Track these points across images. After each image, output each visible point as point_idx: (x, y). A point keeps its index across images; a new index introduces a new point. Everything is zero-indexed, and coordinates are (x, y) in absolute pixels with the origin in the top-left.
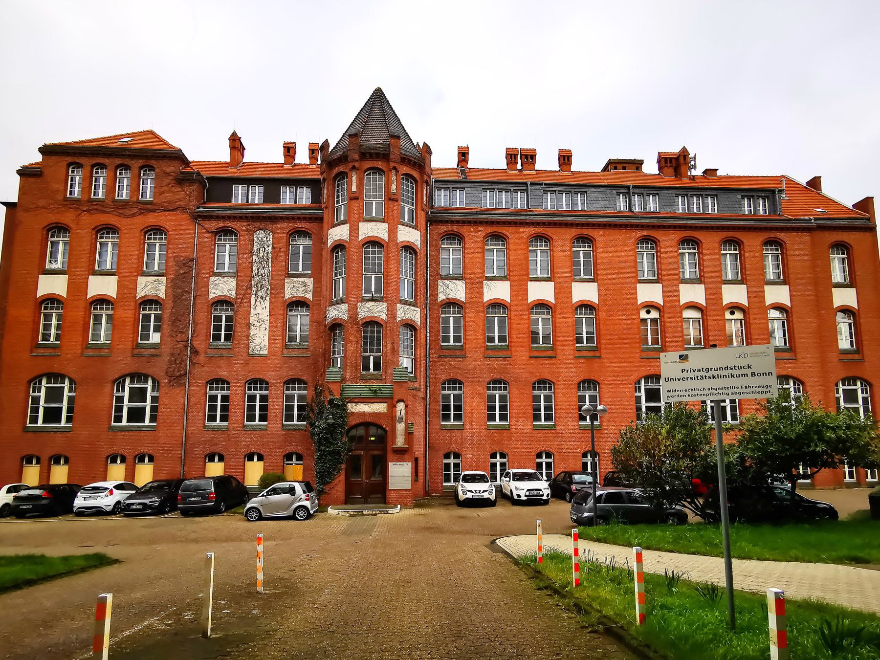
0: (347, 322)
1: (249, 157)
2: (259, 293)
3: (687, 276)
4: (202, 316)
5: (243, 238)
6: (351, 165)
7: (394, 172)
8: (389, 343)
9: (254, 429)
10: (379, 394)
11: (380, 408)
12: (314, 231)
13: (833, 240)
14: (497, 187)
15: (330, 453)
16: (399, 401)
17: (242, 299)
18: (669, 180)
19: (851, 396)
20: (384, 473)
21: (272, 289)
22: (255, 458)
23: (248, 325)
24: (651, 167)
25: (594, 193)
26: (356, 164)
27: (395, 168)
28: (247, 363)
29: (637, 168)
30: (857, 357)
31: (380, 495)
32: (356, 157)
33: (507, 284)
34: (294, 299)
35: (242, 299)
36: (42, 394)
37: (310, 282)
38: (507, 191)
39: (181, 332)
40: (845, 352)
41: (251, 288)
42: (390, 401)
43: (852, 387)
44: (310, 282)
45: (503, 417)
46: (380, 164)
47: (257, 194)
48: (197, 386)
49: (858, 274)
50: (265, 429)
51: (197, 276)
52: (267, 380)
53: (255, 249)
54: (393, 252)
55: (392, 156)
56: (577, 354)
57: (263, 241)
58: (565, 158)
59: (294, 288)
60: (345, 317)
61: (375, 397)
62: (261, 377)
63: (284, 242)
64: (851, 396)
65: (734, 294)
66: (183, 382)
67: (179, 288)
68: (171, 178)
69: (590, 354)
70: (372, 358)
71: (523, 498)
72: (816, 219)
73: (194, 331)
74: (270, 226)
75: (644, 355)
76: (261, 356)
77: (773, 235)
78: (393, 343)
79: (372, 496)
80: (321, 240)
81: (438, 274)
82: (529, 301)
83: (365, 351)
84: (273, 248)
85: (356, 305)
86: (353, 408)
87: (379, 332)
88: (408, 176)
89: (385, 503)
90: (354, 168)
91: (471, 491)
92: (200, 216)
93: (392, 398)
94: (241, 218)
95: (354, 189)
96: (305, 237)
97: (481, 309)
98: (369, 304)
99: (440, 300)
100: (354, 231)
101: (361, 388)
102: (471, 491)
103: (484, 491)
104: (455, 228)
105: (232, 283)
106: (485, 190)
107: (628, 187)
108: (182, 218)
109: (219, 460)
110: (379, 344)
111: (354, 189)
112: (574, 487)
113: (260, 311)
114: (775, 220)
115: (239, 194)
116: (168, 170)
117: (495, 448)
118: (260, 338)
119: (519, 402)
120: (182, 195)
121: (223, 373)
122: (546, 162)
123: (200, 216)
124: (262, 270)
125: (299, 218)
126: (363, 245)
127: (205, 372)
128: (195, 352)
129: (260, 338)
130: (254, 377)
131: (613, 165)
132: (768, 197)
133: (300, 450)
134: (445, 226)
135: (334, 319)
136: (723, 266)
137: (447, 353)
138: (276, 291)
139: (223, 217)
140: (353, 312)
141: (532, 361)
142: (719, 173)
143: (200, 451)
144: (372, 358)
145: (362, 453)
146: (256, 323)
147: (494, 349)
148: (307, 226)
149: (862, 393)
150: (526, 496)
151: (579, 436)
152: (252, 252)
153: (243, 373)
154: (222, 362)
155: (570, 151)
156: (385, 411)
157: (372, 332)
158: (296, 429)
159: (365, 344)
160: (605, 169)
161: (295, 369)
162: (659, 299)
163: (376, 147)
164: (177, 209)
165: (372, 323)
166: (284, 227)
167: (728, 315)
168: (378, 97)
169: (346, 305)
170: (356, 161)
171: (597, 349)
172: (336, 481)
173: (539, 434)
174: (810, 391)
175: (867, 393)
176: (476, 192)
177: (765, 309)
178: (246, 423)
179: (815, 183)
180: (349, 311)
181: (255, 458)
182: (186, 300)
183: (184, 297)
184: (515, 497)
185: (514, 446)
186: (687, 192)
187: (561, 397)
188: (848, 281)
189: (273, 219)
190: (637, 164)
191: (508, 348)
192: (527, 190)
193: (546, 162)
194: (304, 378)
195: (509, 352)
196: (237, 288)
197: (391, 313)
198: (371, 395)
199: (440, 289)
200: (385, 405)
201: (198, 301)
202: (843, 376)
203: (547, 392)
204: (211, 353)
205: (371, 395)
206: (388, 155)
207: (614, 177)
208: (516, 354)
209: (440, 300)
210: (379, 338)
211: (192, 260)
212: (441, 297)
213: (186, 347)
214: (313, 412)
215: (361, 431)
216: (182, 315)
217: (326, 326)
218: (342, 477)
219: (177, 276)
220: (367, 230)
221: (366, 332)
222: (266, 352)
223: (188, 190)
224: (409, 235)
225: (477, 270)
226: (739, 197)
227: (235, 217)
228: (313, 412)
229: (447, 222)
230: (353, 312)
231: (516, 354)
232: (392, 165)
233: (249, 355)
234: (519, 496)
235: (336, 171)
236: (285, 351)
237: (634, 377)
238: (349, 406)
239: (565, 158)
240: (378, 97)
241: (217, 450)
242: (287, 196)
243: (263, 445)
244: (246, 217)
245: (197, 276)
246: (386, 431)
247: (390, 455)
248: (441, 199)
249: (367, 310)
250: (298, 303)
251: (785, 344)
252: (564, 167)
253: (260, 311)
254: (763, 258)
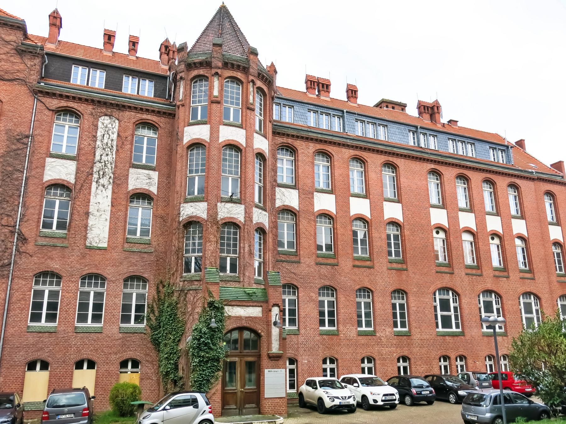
0: (206, 221)
1: (65, 36)
2: (101, 181)
3: (322, 186)
4: (33, 200)
5: (87, 120)
6: (214, 71)
7: (251, 84)
8: (247, 245)
9: (88, 332)
10: (254, 298)
11: (255, 312)
12: (162, 125)
13: (546, 189)
14: (320, 110)
15: (209, 359)
16: (275, 305)
17: (82, 186)
18: (426, 121)
19: (528, 309)
20: (259, 383)
21: (114, 178)
22: (38, 366)
23: (87, 214)
24: (412, 111)
25: (393, 128)
26: (219, 71)
27: (253, 81)
28: (83, 256)
29: (402, 110)
30: (528, 275)
31: (254, 405)
32: (220, 64)
33: (333, 197)
34: (138, 191)
35: (82, 186)
36: (452, 305)
37: (155, 175)
38: (328, 114)
39: (8, 215)
40: (496, 269)
41: (92, 174)
42: (265, 305)
43: (445, 297)
44: (155, 175)
45: (331, 323)
46: (239, 75)
47: (98, 80)
48: (22, 278)
49: (562, 216)
50: (99, 332)
51: (33, 153)
52: (105, 274)
53: (99, 134)
54: (214, 152)
55: (251, 70)
56: (389, 266)
57: (108, 127)
58: (352, 92)
59: (142, 180)
60: (204, 216)
61: (249, 300)
62: (99, 272)
63: (129, 132)
64: (528, 309)
65: (467, 220)
66: (6, 272)
67: (9, 165)
68: (9, 47)
69: (399, 266)
70: (228, 259)
71: (380, 403)
72: (536, 172)
73: (23, 215)
74: (116, 113)
75: (438, 269)
76: (100, 249)
77: (391, 159)
78: (250, 246)
79: (247, 406)
80: (174, 136)
81: (275, 181)
82: (385, 219)
83: (222, 251)
84: (119, 135)
85: (216, 205)
86: (232, 311)
87: (235, 234)
88: (260, 89)
89: (260, 413)
90: (217, 74)
91: (338, 398)
92: (41, 92)
93: (267, 302)
94: (87, 100)
95: (216, 93)
96: (149, 129)
97: (312, 218)
98: (229, 205)
99: (277, 205)
100: (214, 133)
101: (233, 290)
102: (338, 398)
103: (349, 397)
104: (290, 141)
105: (72, 166)
106: (310, 110)
107: (416, 127)
108: (21, 90)
109: (42, 368)
110: (235, 246)
111: (216, 93)
112: (414, 391)
113: (101, 199)
114: (499, 167)
115: (79, 76)
116: (8, 38)
117: (328, 354)
118: (99, 231)
119: (345, 310)
120: (22, 66)
121: (55, 266)
122: (338, 93)
123: (41, 92)
124: (105, 157)
125: (147, 110)
126: (223, 147)
127: (33, 264)
128: (23, 239)
129: (99, 231)
130: (90, 271)
131: (383, 104)
132: (504, 150)
133: (137, 355)
134: (287, 139)
135: (191, 217)
136: (316, 176)
137: (283, 258)
138: (119, 181)
139: (67, 97)
140: (212, 211)
141: (356, 270)
142: (459, 124)
143: (22, 357)
144: (228, 259)
145: (236, 359)
146: (95, 213)
147: (324, 257)
148: (154, 119)
149: (454, 302)
150: (382, 401)
151: (394, 342)
152: (95, 137)
153: (78, 266)
154: (55, 253)
155: (329, 81)
156: (260, 315)
157: (229, 233)
158: (134, 332)
159: (222, 244)
160: (377, 106)
161: (136, 265)
162: (367, 213)
163: (223, 59)
164: (15, 80)
165: (232, 224)
166: (131, 116)
167: (435, 235)
168: (223, 14)
169: (205, 204)
170: (219, 68)
171: (404, 262)
172: (213, 391)
173: (363, 340)
174: (544, 305)
175: (456, 303)
176: (303, 111)
177: (512, 237)
178: (77, 325)
179: (520, 143)
180: (208, 210)
181: (38, 366)
182: (17, 179)
183: (15, 176)
184: (371, 402)
185: (344, 353)
186: (436, 133)
187: (378, 306)
188: (519, 214)
189: (121, 107)
190: (403, 106)
191: (335, 256)
192: (343, 117)
193: (338, 93)
194: (145, 275)
195: (336, 261)
196: (77, 173)
197: (248, 215)
198: (245, 298)
199: (278, 196)
200: (260, 309)
201: (31, 182)
202: (561, 294)
203: (367, 300)
204: (41, 241)
205: (245, 298)
206: (248, 68)
207: (384, 113)
208: (343, 262)
209: (277, 205)
210: (235, 239)
211: (27, 137)
212: (278, 204)
213: (12, 233)
214: (154, 313)
215: (235, 335)
216: (11, 197)
217: (179, 223)
218: (219, 387)
219: (8, 152)
220: (227, 134)
221: (223, 232)
222: (105, 245)
223: (29, 63)
224: (262, 144)
225: (309, 181)
226: (488, 147)
227: (80, 99)
228: (154, 313)
229: (284, 134)
230: (212, 211)
231: (343, 262)
232: (251, 78)
233: (87, 247)
234: (375, 401)
235: (195, 73)
236: (126, 245)
237: (432, 289)
238: (226, 308)
239: (352, 92)
240: (223, 14)
241: (85, 356)
242: (129, 86)
243: (96, 350)
244: (93, 101)
245: (33, 153)
246: (258, 335)
247: (265, 361)
248: (287, 116)
249: (226, 210)
250: (142, 196)
251: (500, 265)
252: (352, 99)
253: (101, 199)
254: (455, 187)
